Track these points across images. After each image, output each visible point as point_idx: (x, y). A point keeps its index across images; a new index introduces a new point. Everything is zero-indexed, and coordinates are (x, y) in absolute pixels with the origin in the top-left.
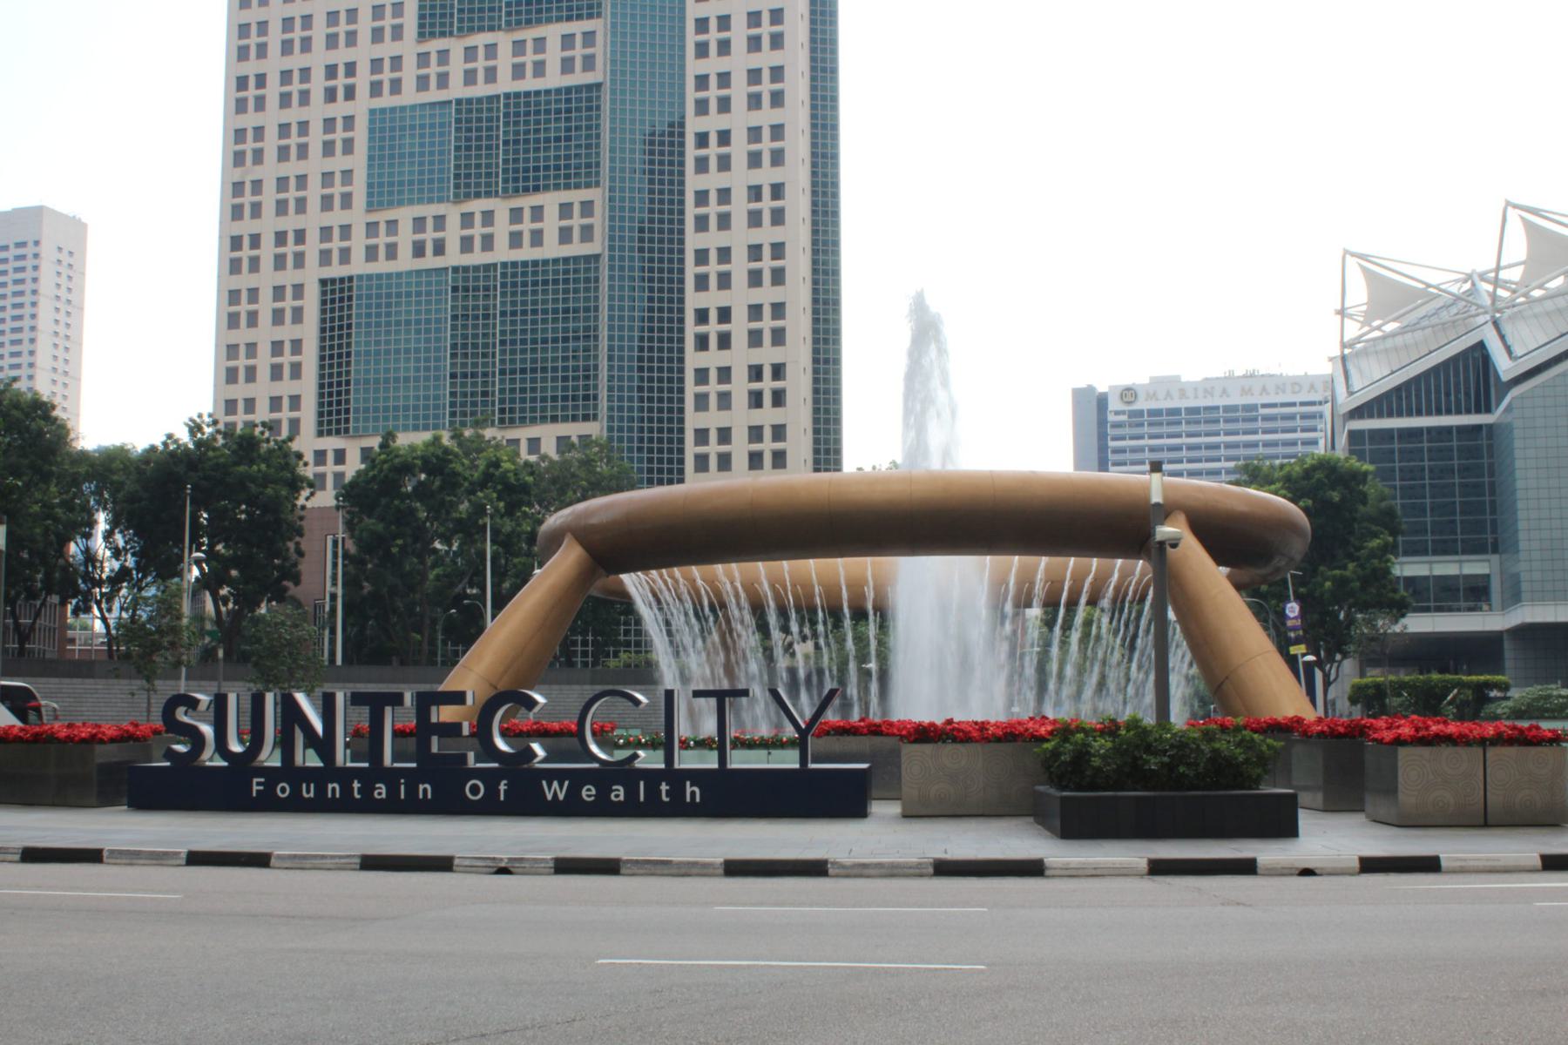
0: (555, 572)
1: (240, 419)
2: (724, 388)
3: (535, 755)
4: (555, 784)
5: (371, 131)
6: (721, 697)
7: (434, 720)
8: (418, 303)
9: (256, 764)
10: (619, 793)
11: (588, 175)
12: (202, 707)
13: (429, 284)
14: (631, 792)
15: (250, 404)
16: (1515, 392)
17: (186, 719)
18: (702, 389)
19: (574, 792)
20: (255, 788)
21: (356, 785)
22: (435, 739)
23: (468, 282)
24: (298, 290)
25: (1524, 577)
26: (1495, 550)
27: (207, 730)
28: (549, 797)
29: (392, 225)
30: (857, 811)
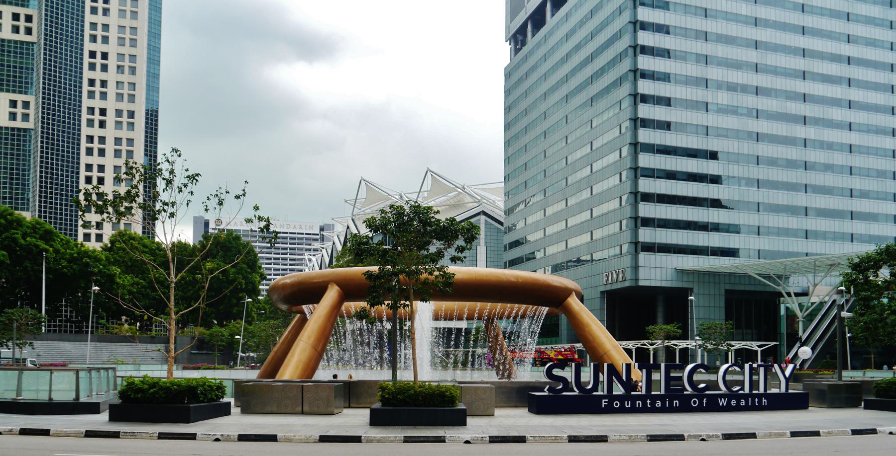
19: (729, 403)
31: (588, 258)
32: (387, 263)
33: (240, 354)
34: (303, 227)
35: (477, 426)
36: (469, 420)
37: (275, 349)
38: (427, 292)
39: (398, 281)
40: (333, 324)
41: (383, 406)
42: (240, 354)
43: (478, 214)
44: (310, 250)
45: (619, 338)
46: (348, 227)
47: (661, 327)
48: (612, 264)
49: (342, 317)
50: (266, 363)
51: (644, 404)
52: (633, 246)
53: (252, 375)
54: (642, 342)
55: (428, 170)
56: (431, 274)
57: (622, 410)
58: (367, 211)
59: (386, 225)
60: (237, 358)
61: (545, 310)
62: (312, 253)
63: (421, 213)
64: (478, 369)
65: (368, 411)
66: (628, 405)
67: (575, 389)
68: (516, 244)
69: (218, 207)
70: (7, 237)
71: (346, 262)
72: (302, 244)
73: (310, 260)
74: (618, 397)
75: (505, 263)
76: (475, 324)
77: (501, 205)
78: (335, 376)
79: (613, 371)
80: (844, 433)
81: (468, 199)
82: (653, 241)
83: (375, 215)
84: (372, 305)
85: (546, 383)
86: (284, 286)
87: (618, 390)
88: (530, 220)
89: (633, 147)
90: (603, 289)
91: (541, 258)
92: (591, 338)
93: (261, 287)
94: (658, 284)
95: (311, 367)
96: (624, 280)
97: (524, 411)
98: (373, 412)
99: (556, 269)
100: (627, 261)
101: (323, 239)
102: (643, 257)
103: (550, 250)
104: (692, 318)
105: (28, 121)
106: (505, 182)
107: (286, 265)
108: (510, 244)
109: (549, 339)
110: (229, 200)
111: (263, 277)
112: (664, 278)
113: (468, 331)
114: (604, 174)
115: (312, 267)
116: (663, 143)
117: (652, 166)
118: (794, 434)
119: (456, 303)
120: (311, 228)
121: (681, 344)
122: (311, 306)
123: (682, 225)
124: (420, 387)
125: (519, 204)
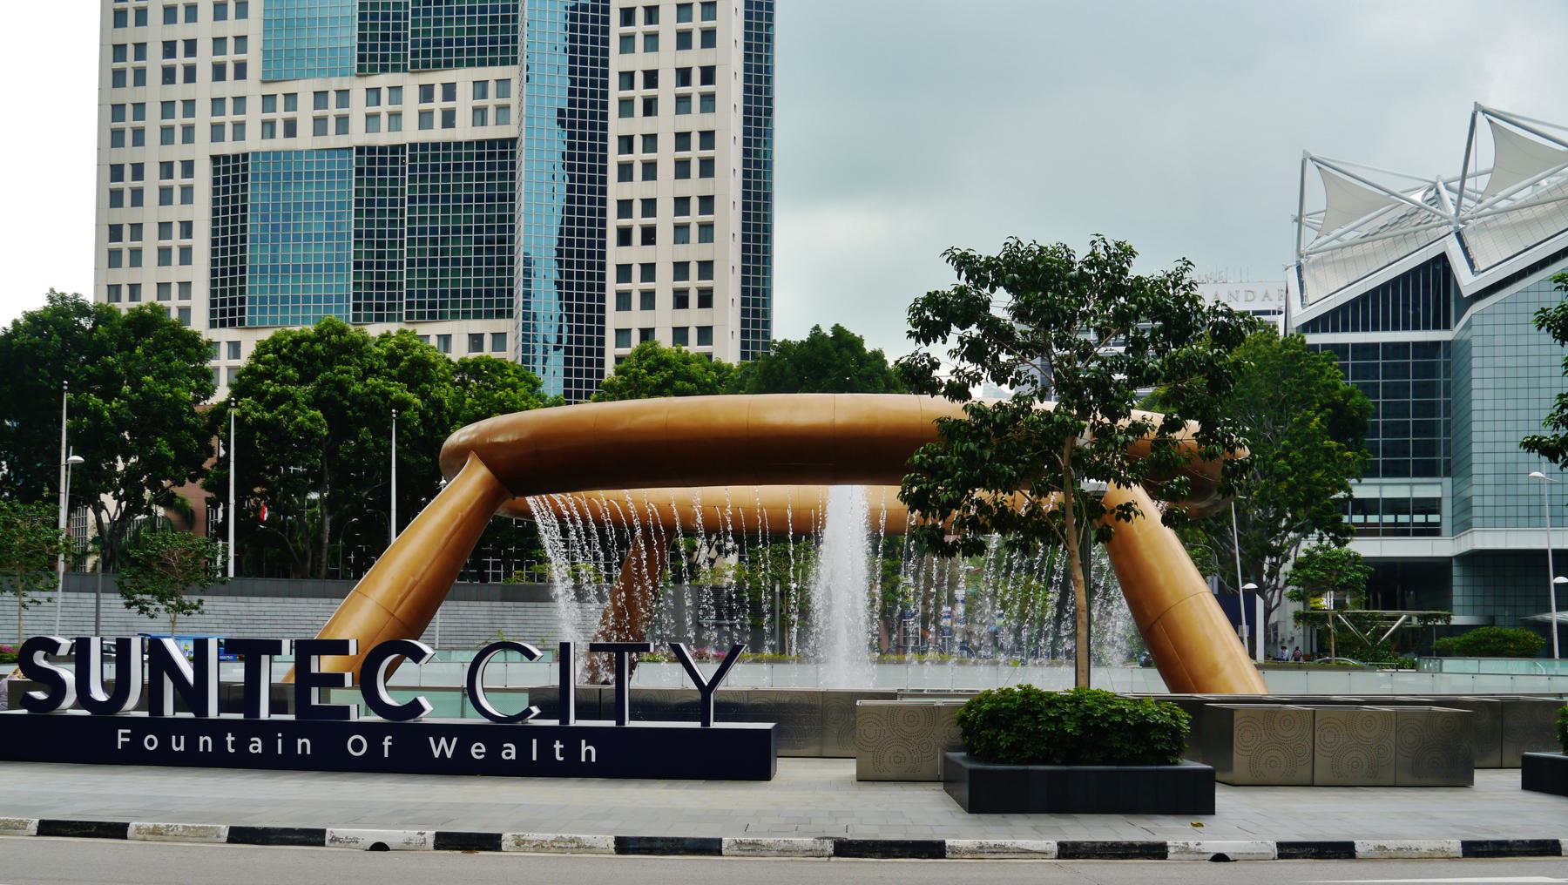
0: (462, 489)
1: (124, 306)
2: (648, 286)
3: (423, 710)
4: (443, 741)
5: (266, 53)
6: (618, 650)
7: (314, 670)
8: (320, 185)
9: (120, 714)
10: (510, 752)
11: (504, 50)
12: (63, 652)
13: (331, 164)
14: (524, 750)
15: (135, 290)
16: (1476, 308)
17: (45, 664)
18: (624, 286)
19: (463, 750)
20: (120, 739)
21: (230, 738)
22: (315, 691)
23: (375, 161)
24: (188, 168)
25: (1476, 501)
26: (1447, 473)
27: (67, 674)
28: (437, 754)
29: (291, 98)
30: (758, 770)
35: (1247, 818)
36: (1224, 798)
55: (1479, 109)
64: (771, 661)
66: (178, 746)
70: (326, 381)
80: (204, 835)
105: (507, 122)
118: (48, 828)
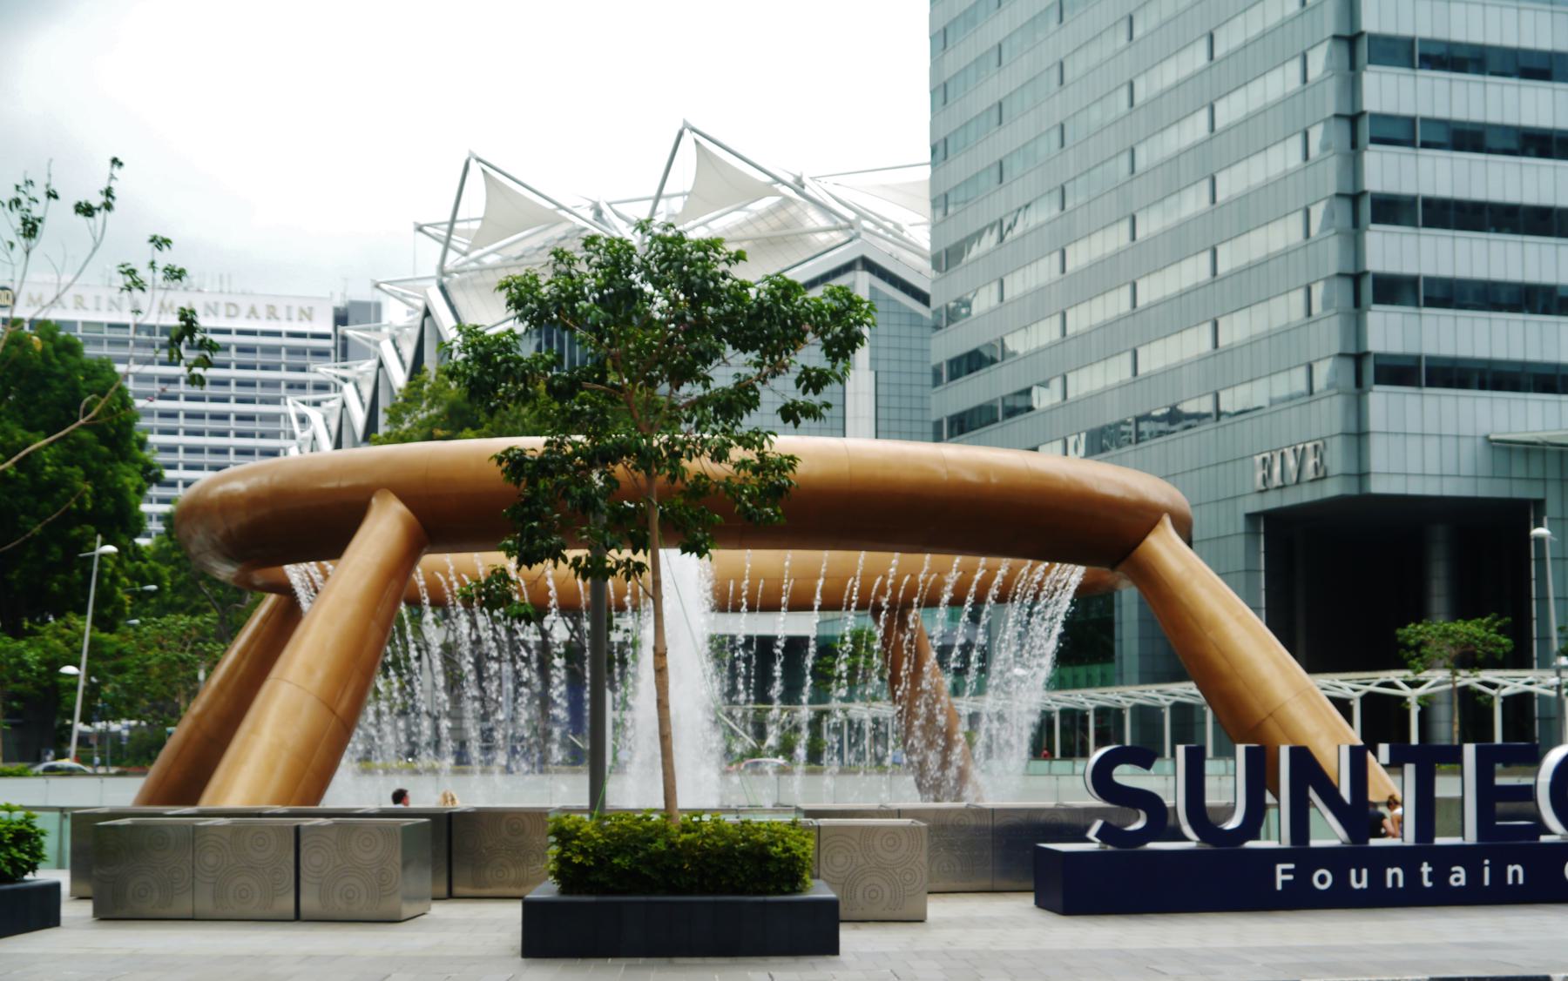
20: (1280, 878)
31: (1206, 405)
32: (570, 422)
33: (79, 727)
34: (281, 313)
36: (848, 937)
37: (197, 707)
38: (704, 519)
39: (610, 479)
40: (385, 629)
41: (563, 891)
42: (79, 727)
43: (848, 267)
44: (302, 386)
45: (1313, 665)
46: (427, 313)
47: (1439, 627)
48: (1283, 428)
49: (414, 602)
50: (164, 756)
51: (1413, 876)
52: (1349, 366)
53: (117, 793)
54: (1384, 676)
55: (687, 126)
56: (720, 455)
57: (1341, 899)
58: (491, 260)
59: (573, 299)
60: (66, 740)
61: (1074, 575)
62: (311, 396)
63: (681, 262)
65: (512, 913)
66: (1323, 880)
67: (1187, 830)
68: (972, 362)
69: (20, 243)
71: (422, 425)
72: (277, 368)
73: (303, 420)
74: (1327, 857)
75: (938, 424)
76: (848, 623)
77: (922, 237)
78: (399, 796)
79: (1306, 766)
81: (815, 219)
82: (1411, 349)
83: (537, 269)
84: (527, 559)
85: (1091, 813)
86: (227, 505)
87: (1327, 832)
88: (1016, 286)
89: (1343, 48)
90: (1255, 505)
91: (1052, 408)
92: (1223, 665)
93: (145, 508)
94: (1431, 489)
95: (315, 771)
96: (1321, 477)
97: (1021, 906)
98: (534, 914)
99: (1101, 442)
100: (1329, 415)
101: (345, 350)
102: (1383, 401)
103: (1085, 382)
104: (1543, 599)
106: (934, 164)
107: (225, 434)
108: (951, 362)
109: (1081, 671)
110: (58, 218)
111: (152, 476)
112: (1450, 468)
113: (827, 648)
114: (1251, 136)
115: (311, 440)
116: (1441, 35)
117: (1407, 110)
119: (826, 554)
120: (307, 314)
121: (1511, 682)
122: (312, 567)
123: (1504, 299)
124: (685, 829)
125: (979, 234)
